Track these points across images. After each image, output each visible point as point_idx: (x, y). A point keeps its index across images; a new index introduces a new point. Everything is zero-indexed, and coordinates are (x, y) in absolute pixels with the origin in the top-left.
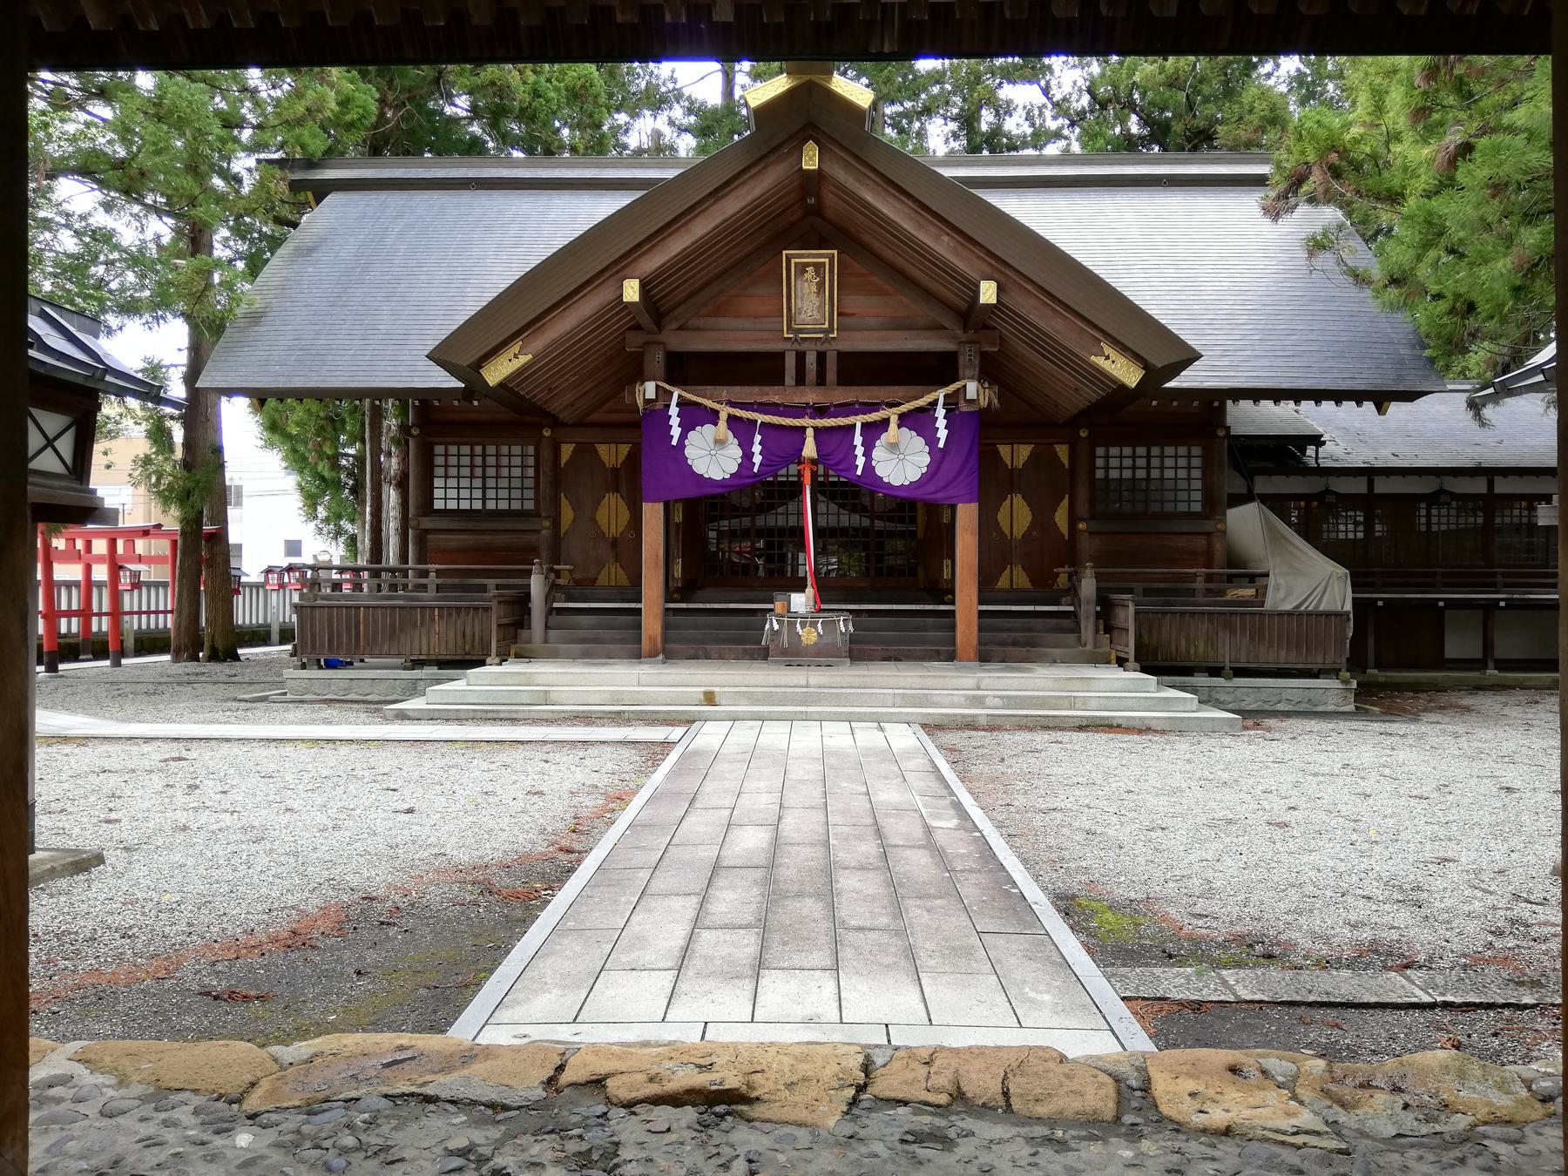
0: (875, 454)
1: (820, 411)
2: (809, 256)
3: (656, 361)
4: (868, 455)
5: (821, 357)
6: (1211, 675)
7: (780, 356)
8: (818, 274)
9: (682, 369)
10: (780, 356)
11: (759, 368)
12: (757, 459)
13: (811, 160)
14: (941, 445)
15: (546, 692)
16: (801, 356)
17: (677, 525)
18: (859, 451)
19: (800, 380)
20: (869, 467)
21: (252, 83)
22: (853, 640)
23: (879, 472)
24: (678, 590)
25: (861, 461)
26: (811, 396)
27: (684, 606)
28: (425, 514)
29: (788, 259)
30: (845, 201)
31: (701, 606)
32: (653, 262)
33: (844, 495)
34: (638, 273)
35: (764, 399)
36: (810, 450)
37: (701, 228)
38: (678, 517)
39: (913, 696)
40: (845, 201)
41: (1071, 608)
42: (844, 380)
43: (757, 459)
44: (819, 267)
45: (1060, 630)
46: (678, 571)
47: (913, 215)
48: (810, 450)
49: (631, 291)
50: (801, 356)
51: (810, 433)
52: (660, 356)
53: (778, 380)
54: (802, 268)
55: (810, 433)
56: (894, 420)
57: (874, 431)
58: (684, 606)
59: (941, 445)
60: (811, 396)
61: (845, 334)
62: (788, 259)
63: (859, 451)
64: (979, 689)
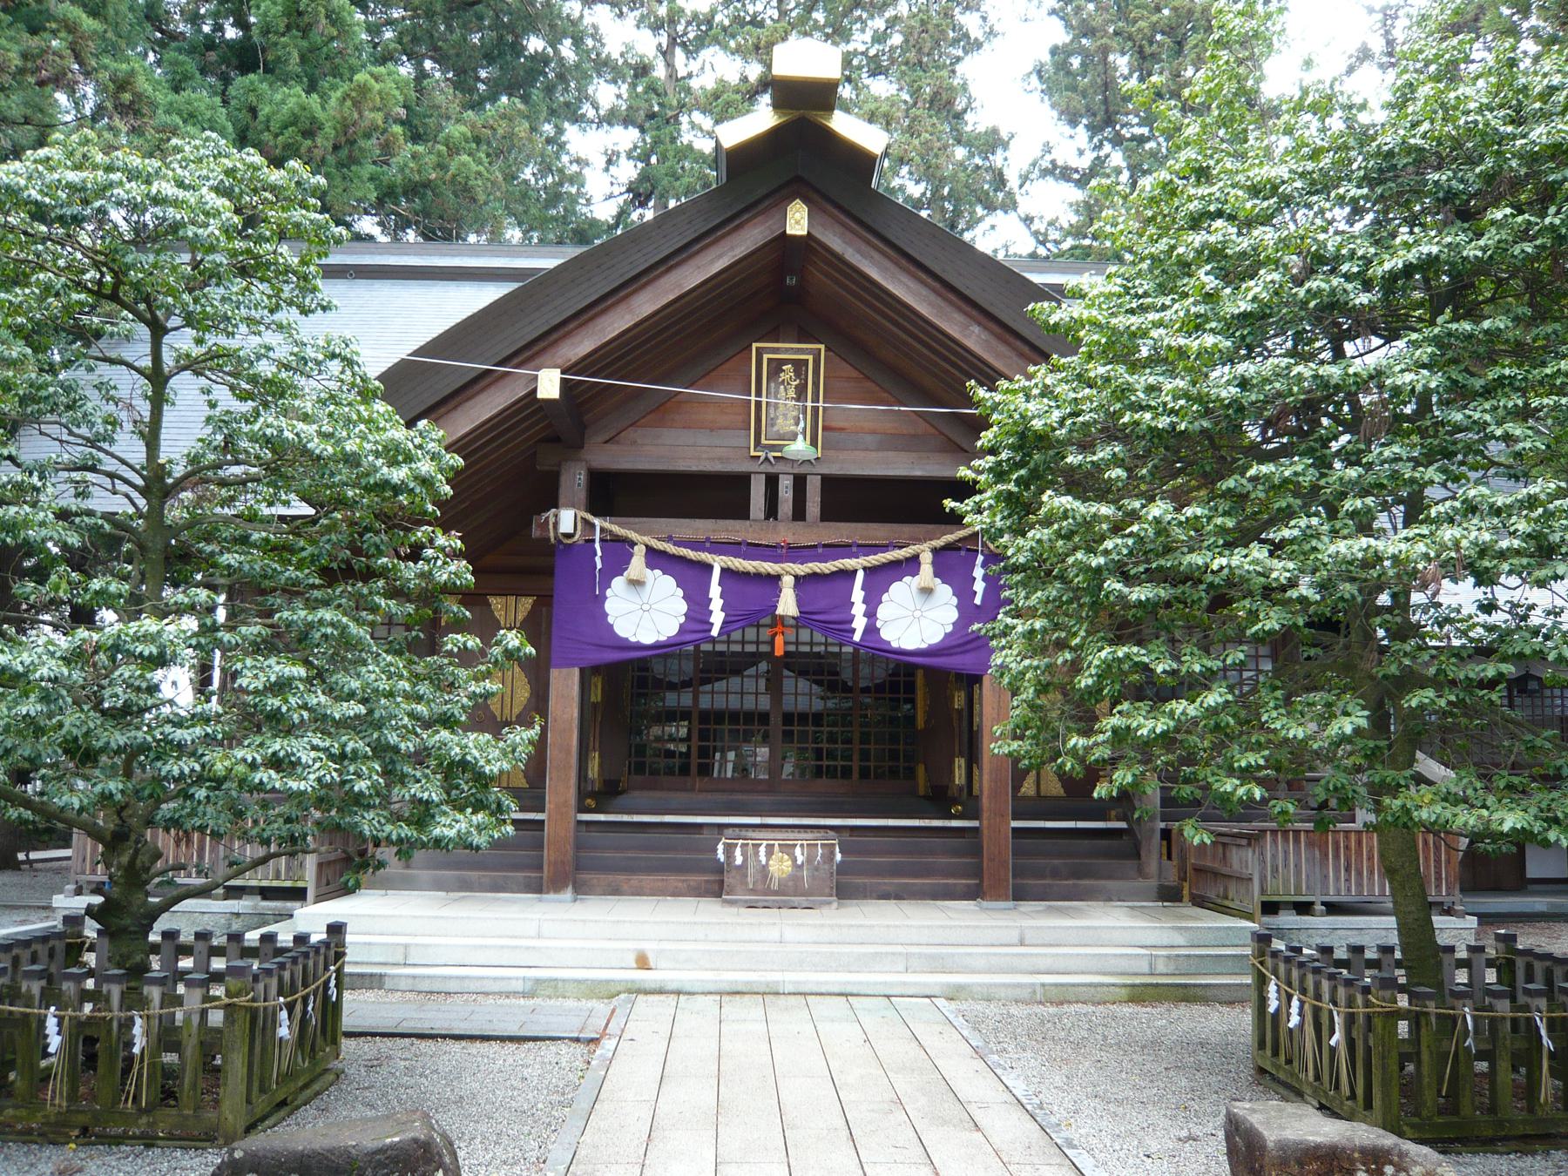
0: (882, 612)
1: (795, 553)
2: (787, 351)
3: (575, 480)
4: (871, 615)
5: (800, 482)
6: (1299, 913)
7: (743, 480)
8: (798, 373)
9: (610, 493)
10: (743, 480)
11: (719, 495)
12: (717, 618)
13: (798, 220)
14: (978, 601)
15: (406, 946)
16: (772, 481)
17: (595, 705)
18: (859, 609)
19: (772, 511)
20: (871, 630)
21: (185, 619)
22: (842, 869)
23: (885, 635)
24: (593, 795)
25: (859, 624)
26: (786, 532)
27: (602, 817)
28: (1401, 1055)
29: (760, 352)
30: (837, 282)
31: (626, 818)
32: (582, 345)
33: (819, 670)
34: (560, 361)
35: (722, 536)
36: (787, 605)
37: (646, 304)
38: (596, 696)
39: (932, 957)
40: (837, 282)
41: (1123, 825)
42: (830, 513)
43: (717, 618)
44: (800, 366)
45: (1108, 854)
46: (594, 770)
47: (933, 297)
48: (787, 605)
49: (549, 385)
50: (772, 481)
51: (788, 581)
52: (582, 478)
53: (742, 512)
54: (776, 367)
55: (788, 581)
56: (926, 558)
57: (880, 579)
58: (602, 817)
59: (978, 601)
60: (786, 532)
61: (831, 453)
62: (760, 352)
63: (859, 609)
64: (1022, 944)
